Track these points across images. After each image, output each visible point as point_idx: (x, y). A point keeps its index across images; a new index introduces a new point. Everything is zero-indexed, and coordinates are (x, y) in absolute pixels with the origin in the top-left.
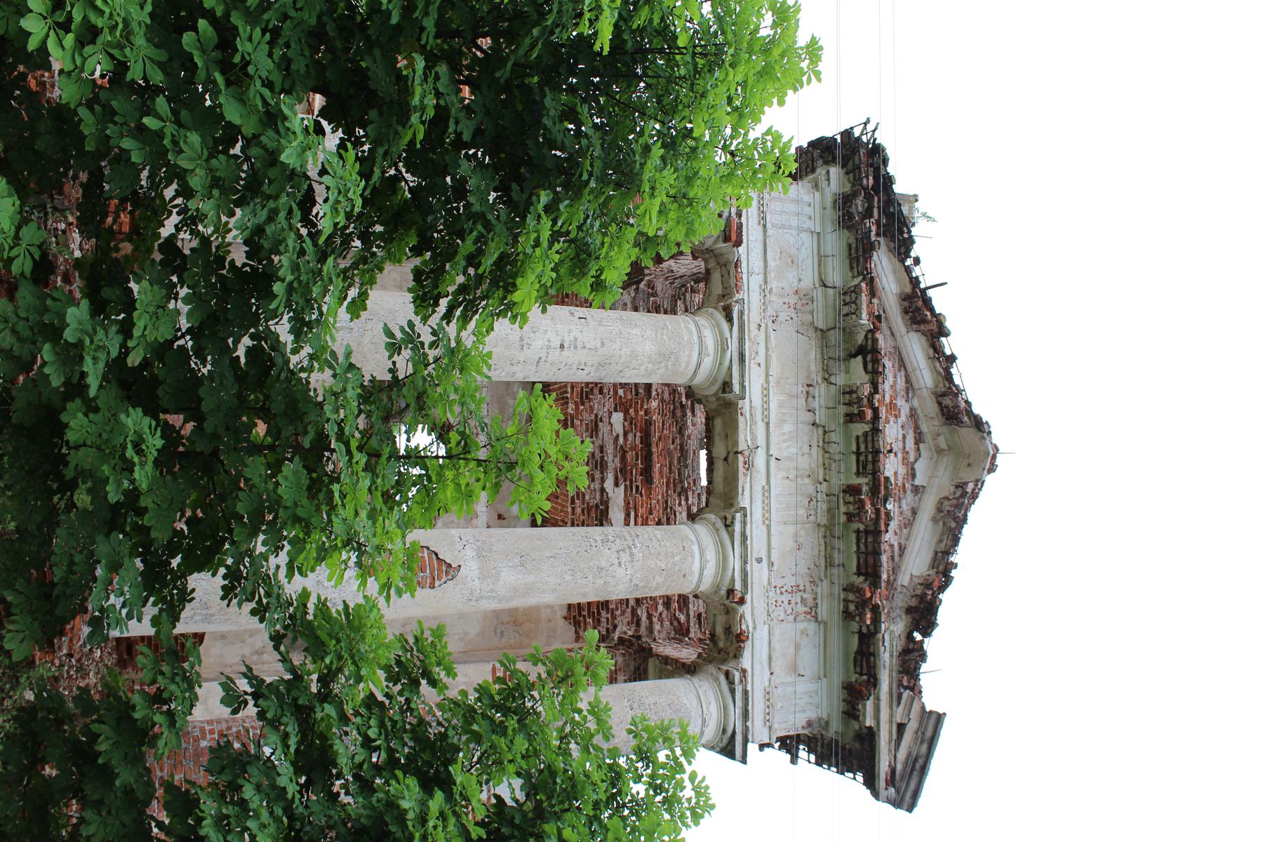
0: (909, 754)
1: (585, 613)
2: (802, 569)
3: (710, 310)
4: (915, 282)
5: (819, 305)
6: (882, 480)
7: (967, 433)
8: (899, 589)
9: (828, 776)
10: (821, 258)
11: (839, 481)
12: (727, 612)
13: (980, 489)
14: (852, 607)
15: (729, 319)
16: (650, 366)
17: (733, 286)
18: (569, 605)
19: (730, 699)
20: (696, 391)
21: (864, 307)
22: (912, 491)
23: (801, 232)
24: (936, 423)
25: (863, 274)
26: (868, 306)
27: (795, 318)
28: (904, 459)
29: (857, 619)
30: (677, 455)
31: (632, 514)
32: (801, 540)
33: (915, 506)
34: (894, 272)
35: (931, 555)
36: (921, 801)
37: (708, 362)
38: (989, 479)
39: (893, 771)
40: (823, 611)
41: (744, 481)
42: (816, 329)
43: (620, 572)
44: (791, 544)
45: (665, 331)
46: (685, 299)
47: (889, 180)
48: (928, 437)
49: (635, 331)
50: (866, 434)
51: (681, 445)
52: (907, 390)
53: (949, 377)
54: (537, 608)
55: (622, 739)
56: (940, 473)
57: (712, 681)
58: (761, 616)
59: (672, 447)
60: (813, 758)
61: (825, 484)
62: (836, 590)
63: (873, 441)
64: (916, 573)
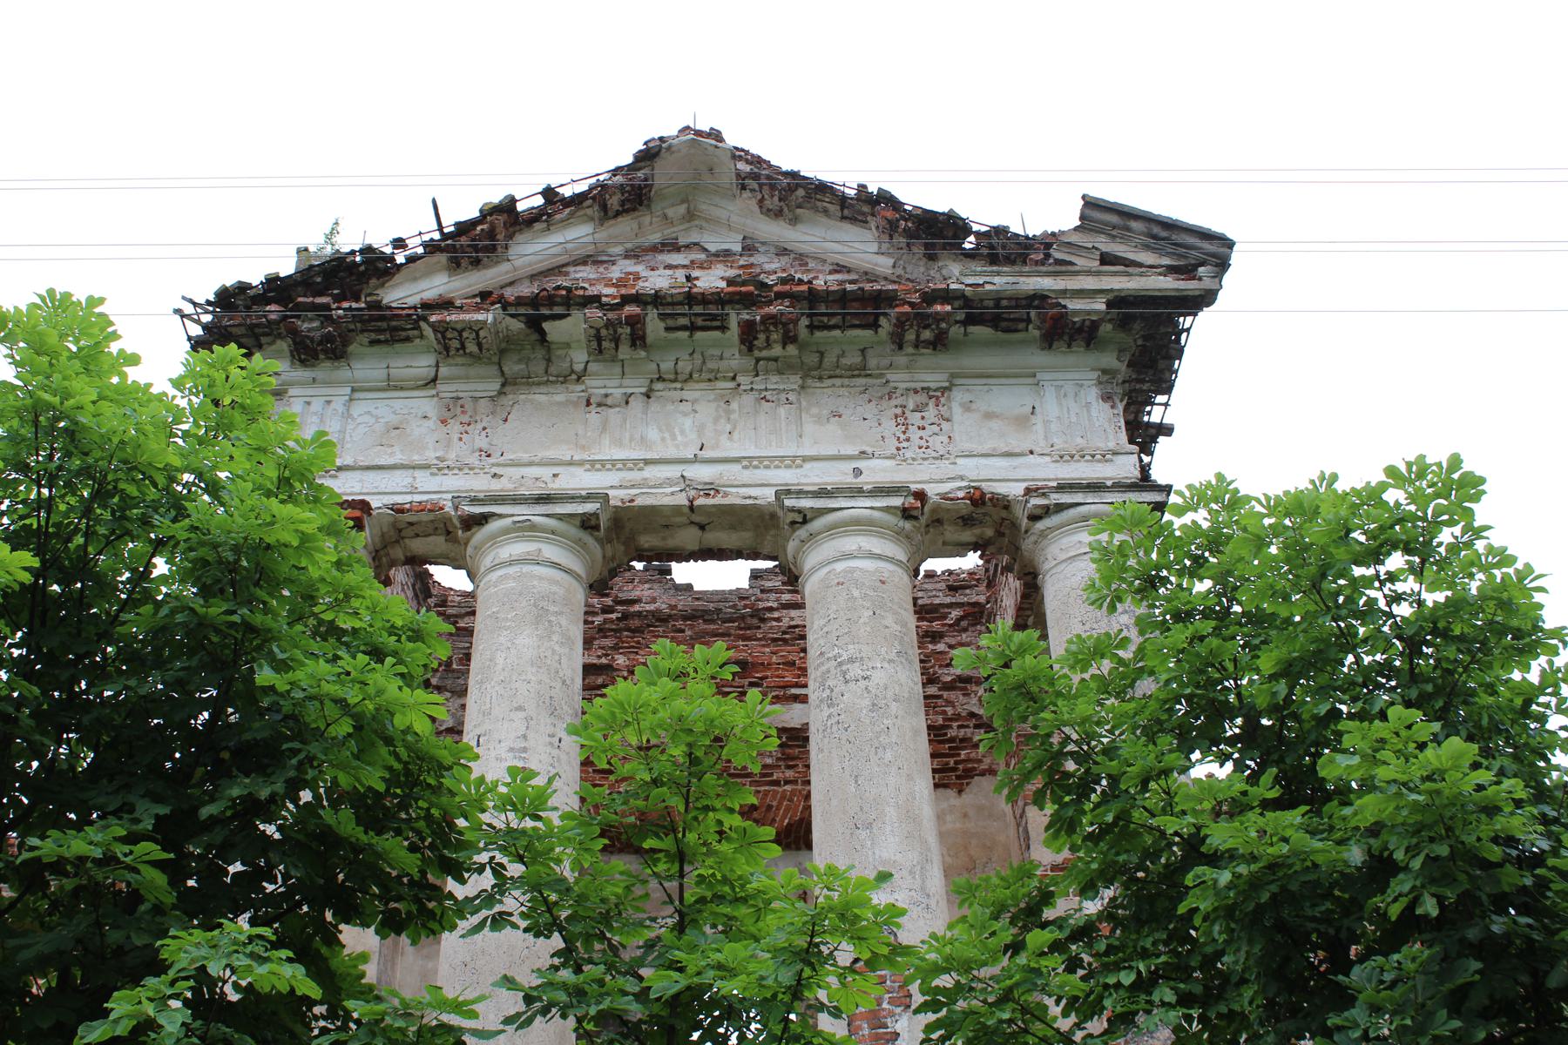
0: (1147, 247)
1: (952, 762)
2: (870, 410)
3: (469, 550)
4: (431, 247)
5: (464, 389)
6: (731, 289)
7: (663, 175)
8: (899, 271)
9: (1189, 370)
10: (393, 385)
11: (735, 359)
12: (939, 522)
13: (747, 152)
14: (927, 335)
15: (483, 519)
16: (555, 638)
17: (431, 516)
18: (936, 786)
19: (1072, 512)
20: (596, 576)
21: (467, 317)
22: (751, 255)
23: (350, 416)
24: (647, 219)
25: (416, 321)
26: (468, 312)
27: (484, 424)
28: (702, 268)
29: (944, 325)
30: (701, 625)
31: (794, 691)
32: (825, 412)
33: (773, 250)
34: (415, 279)
35: (847, 226)
36: (1216, 227)
37: (551, 552)
38: (732, 139)
39: (1172, 270)
40: (935, 379)
41: (735, 497)
42: (501, 393)
43: (878, 677)
44: (833, 427)
45: (501, 615)
46: (456, 616)
47: (272, 281)
48: (669, 232)
49: (500, 661)
50: (662, 317)
51: (685, 618)
52: (597, 263)
53: (578, 200)
54: (942, 835)
55: (1125, 619)
56: (723, 214)
57: (1045, 542)
58: (944, 468)
59: (688, 633)
60: (1161, 399)
61: (740, 379)
62: (901, 359)
63: (673, 304)
64: (874, 247)
